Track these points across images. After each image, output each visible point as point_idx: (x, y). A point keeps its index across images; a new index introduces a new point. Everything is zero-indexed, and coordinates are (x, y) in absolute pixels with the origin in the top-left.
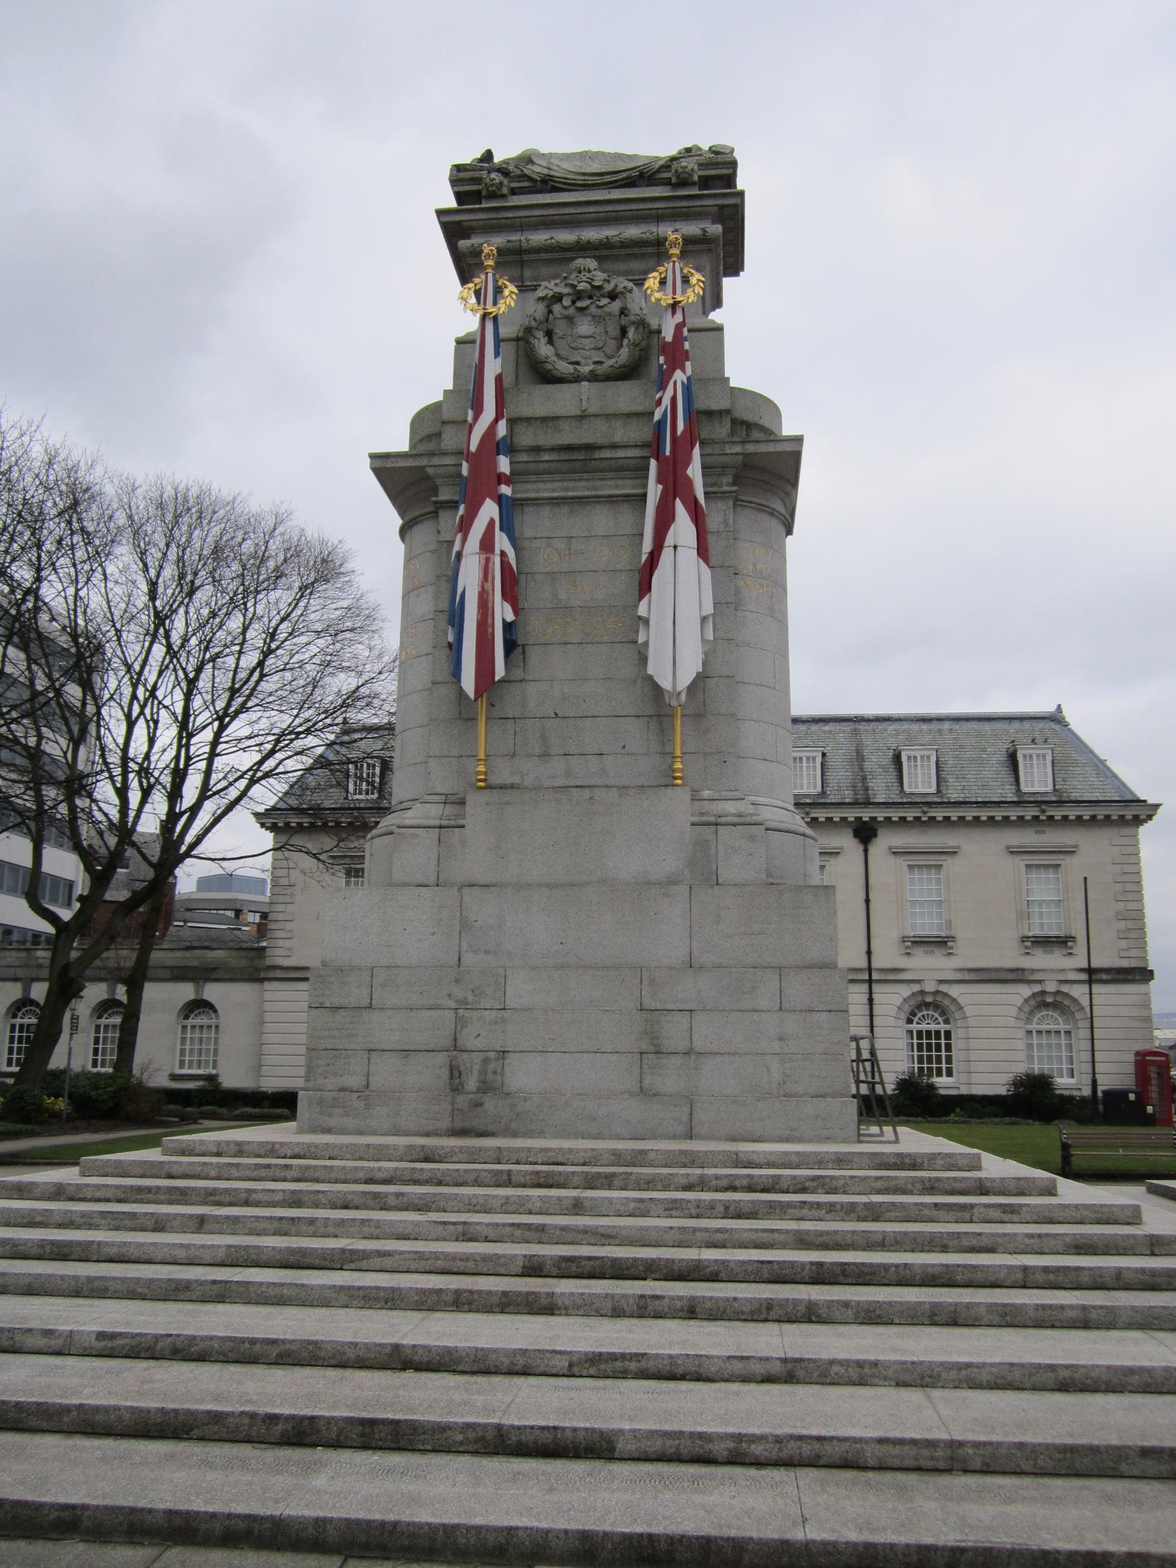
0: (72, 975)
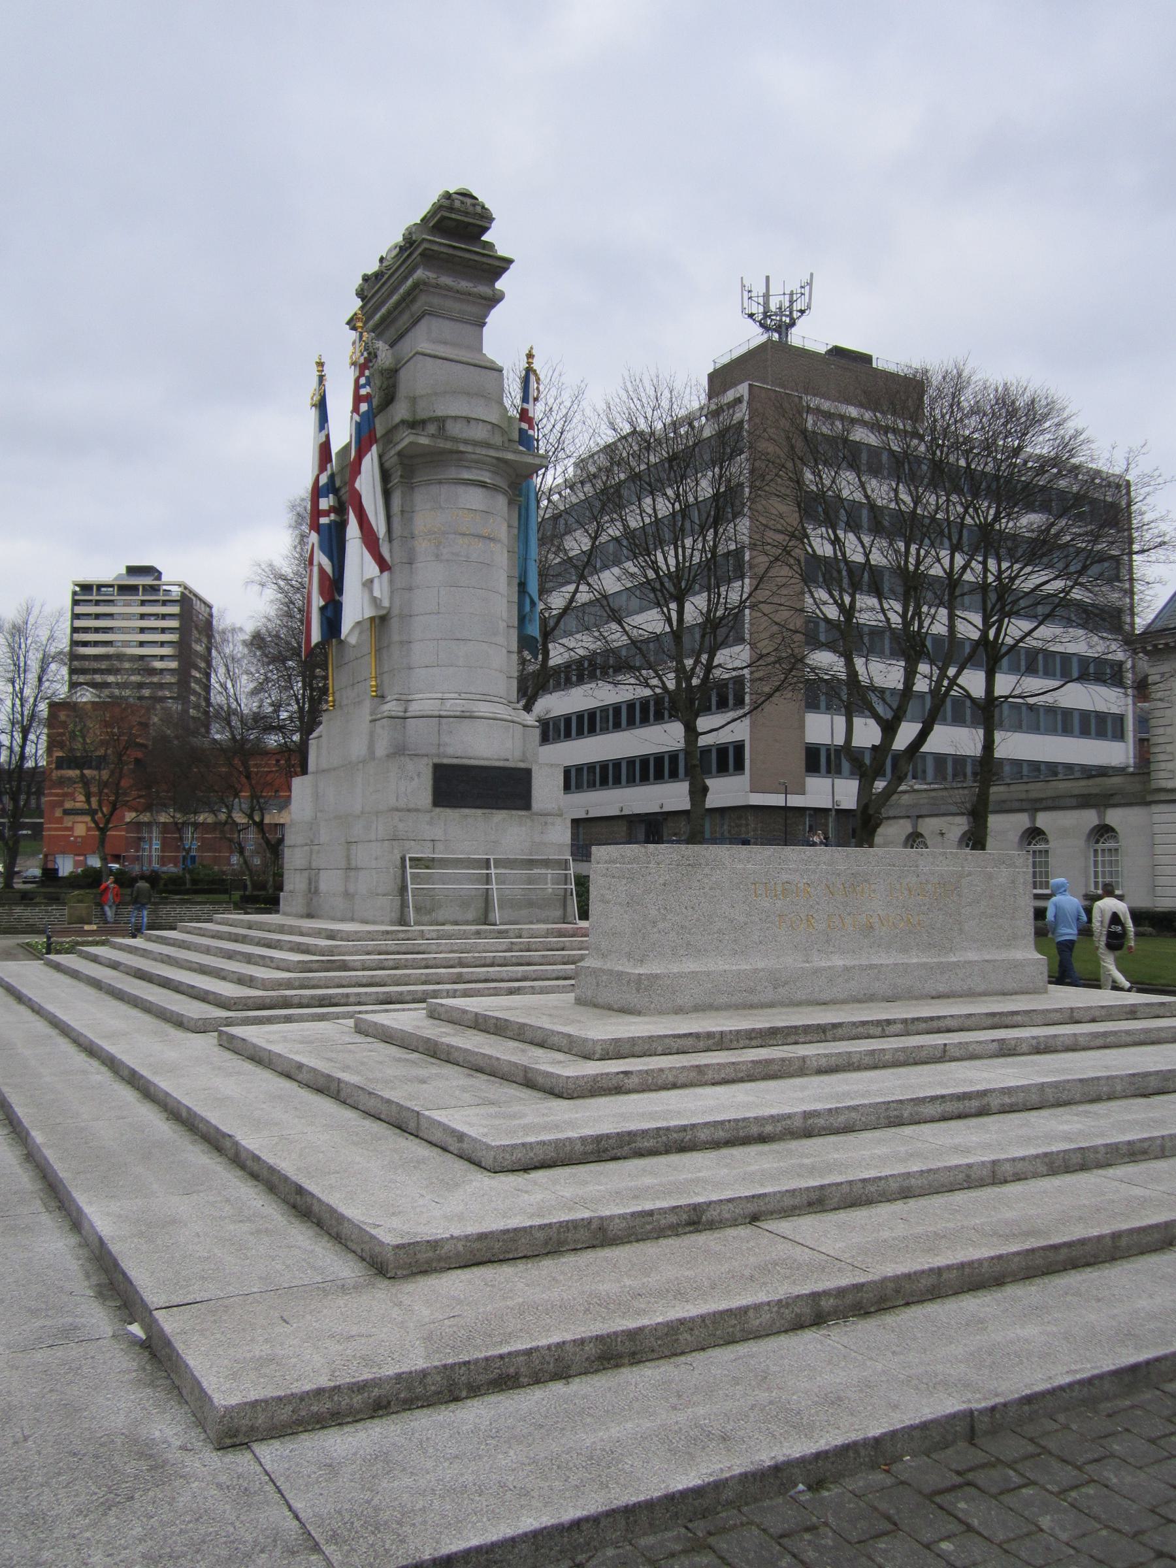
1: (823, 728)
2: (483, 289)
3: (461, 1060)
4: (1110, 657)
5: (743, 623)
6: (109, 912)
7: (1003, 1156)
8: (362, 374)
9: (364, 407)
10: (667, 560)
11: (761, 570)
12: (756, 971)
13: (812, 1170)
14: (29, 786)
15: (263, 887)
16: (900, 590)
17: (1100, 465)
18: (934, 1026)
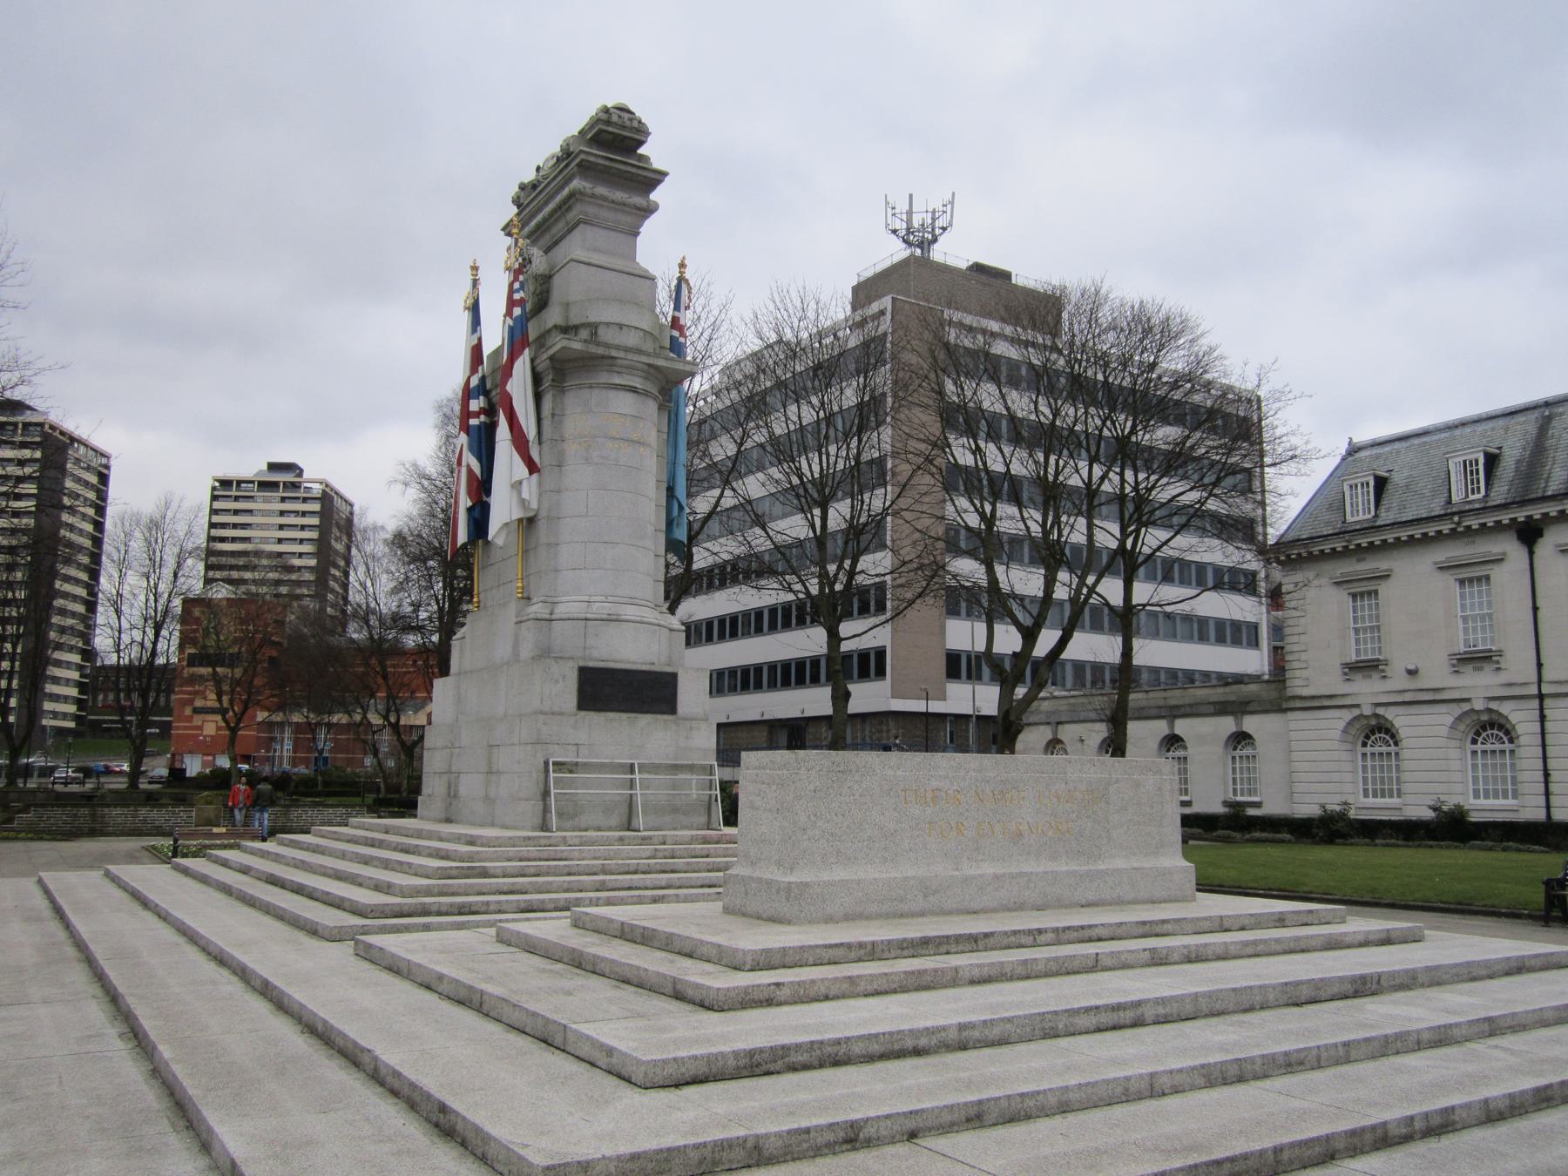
0: (1012, 718)
1: (964, 634)
2: (637, 200)
3: (607, 971)
4: (1244, 566)
5: (885, 528)
6: (238, 816)
7: (1161, 1068)
8: (516, 279)
9: (517, 311)
10: (811, 466)
11: (902, 479)
12: (906, 879)
13: (969, 1085)
14: (159, 684)
15: (397, 790)
16: (1039, 499)
17: (1233, 380)
18: (1086, 935)
